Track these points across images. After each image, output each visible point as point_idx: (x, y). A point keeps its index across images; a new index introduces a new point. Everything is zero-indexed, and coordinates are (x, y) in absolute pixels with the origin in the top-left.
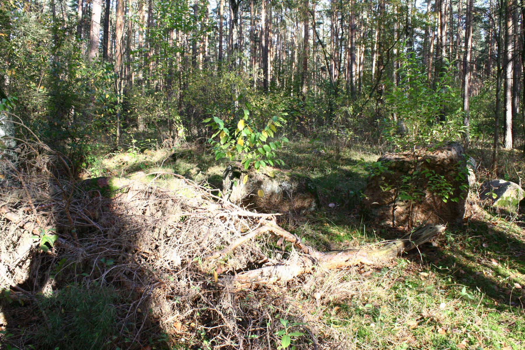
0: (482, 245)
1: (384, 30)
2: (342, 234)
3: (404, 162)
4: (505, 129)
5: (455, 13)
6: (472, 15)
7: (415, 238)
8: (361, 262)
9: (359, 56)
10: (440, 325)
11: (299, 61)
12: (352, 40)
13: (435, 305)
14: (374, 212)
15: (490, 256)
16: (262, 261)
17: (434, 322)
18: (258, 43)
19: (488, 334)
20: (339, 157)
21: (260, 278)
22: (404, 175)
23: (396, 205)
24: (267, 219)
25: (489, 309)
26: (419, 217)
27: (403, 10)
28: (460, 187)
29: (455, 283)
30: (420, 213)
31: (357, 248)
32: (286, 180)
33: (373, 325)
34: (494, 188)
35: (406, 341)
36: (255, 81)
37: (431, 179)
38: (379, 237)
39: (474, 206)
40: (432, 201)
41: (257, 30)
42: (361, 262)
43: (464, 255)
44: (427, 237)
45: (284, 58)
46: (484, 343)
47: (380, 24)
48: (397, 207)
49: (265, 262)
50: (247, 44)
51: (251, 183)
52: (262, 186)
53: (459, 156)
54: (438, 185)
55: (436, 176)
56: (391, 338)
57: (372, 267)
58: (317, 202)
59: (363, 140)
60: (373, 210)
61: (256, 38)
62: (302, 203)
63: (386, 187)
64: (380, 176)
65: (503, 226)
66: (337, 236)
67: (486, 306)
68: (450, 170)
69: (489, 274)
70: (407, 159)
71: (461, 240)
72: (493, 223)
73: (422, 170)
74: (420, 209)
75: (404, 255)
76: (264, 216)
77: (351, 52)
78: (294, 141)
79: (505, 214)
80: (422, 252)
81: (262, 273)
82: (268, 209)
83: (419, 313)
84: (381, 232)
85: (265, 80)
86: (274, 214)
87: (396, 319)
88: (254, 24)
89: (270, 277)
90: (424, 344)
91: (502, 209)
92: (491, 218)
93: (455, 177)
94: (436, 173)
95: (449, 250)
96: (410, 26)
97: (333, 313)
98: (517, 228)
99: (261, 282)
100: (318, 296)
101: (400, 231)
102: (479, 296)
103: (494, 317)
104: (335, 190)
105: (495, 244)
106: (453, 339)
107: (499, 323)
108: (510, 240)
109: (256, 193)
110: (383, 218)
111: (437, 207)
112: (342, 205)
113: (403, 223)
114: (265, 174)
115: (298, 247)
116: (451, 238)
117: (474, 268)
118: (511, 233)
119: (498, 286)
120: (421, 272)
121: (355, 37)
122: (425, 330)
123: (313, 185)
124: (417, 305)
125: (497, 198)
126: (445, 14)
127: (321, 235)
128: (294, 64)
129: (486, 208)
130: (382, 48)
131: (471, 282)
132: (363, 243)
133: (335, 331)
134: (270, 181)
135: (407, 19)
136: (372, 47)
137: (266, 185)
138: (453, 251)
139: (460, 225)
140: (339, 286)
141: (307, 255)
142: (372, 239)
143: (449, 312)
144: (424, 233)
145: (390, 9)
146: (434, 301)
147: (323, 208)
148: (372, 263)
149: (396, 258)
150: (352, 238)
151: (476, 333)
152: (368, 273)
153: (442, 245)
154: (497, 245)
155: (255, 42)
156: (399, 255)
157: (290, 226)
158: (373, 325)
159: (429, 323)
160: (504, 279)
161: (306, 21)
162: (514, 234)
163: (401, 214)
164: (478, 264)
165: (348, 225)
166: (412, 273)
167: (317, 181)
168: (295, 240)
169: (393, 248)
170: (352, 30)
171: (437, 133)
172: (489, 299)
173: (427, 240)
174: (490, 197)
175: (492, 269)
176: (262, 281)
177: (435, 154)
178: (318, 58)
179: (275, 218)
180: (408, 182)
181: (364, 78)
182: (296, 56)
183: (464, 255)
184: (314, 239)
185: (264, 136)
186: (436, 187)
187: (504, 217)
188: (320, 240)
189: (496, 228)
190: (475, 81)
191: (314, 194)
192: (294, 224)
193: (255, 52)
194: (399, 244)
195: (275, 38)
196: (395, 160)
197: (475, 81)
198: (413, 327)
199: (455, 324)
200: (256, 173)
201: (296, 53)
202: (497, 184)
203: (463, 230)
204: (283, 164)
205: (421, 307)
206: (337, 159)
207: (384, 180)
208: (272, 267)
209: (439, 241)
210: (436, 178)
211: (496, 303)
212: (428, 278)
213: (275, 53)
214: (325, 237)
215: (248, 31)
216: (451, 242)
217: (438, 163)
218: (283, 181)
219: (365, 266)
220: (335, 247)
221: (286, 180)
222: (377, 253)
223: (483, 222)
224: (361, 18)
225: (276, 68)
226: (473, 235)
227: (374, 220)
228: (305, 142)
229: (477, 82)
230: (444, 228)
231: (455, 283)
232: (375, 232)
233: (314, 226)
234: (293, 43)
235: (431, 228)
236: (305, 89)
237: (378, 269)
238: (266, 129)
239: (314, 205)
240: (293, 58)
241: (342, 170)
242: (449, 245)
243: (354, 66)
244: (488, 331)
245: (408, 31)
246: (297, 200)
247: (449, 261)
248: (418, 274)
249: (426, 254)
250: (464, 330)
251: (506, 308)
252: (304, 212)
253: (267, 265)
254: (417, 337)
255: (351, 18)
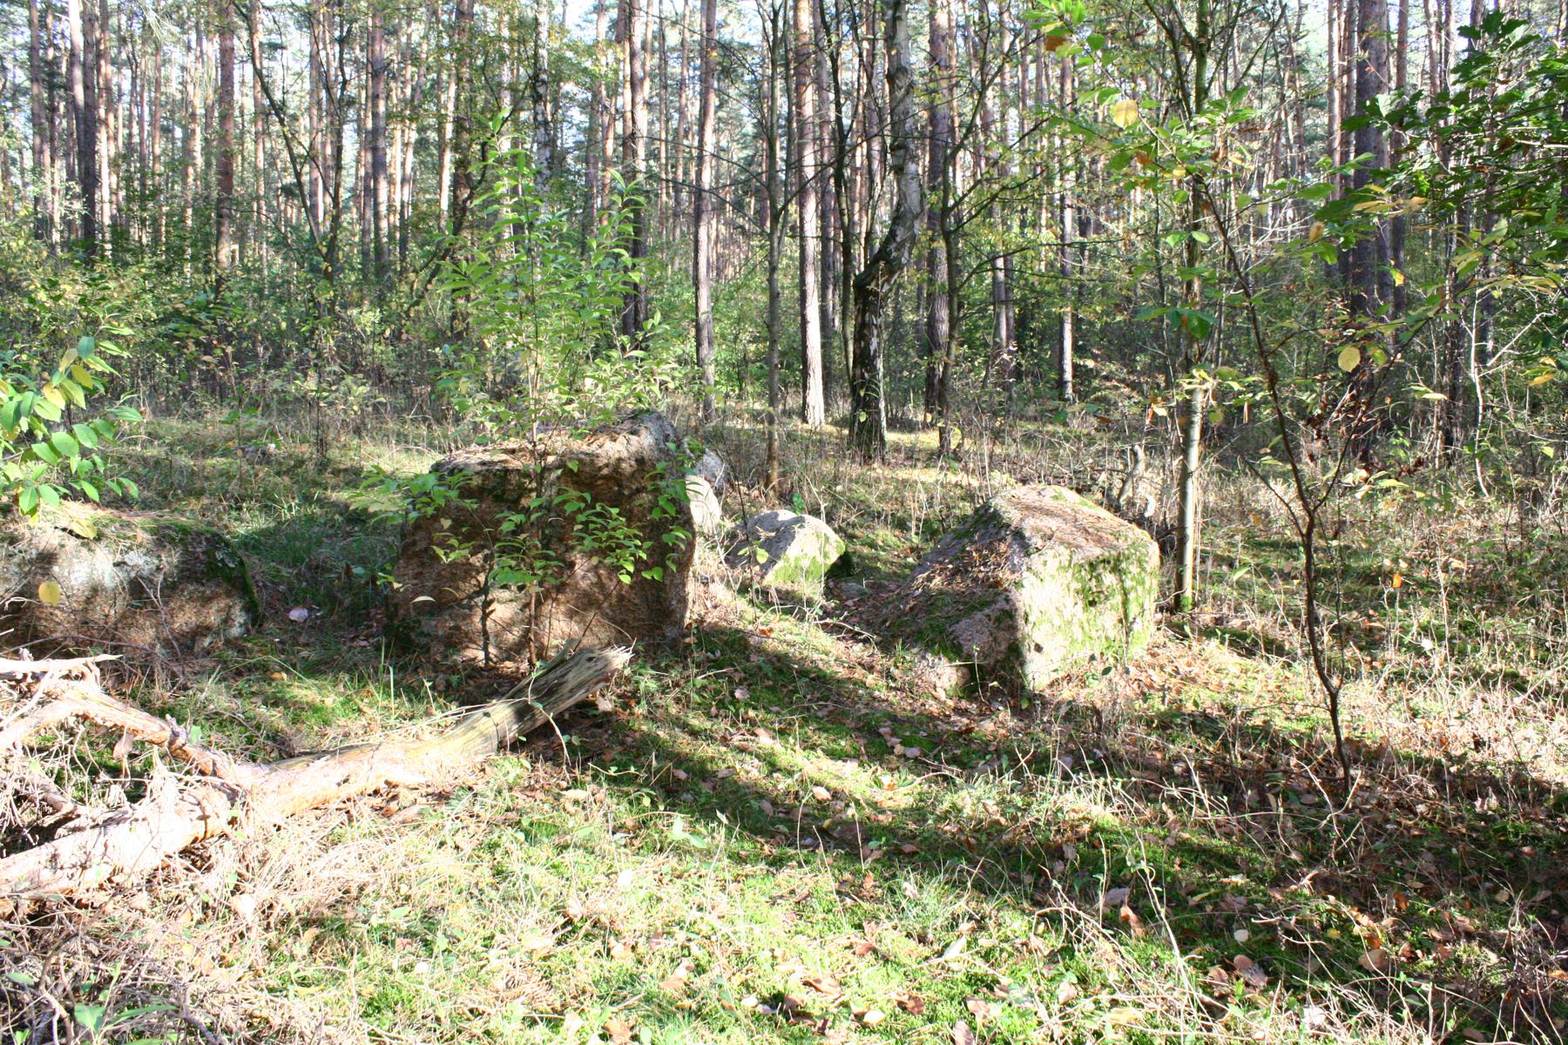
0: (732, 694)
1: (470, 81)
2: (329, 702)
3: (506, 471)
4: (805, 374)
5: (674, 49)
6: (719, 60)
7: (547, 692)
8: (387, 783)
9: (399, 157)
10: (618, 935)
11: (208, 164)
12: (375, 106)
13: (604, 880)
14: (428, 624)
15: (753, 723)
16: (58, 816)
17: (600, 930)
18: (62, 92)
19: (743, 935)
20: (323, 465)
21: (46, 875)
22: (509, 509)
23: (492, 601)
24: (67, 677)
25: (748, 868)
26: (559, 628)
27: (526, 28)
28: (665, 538)
29: (662, 808)
30: (561, 617)
31: (375, 738)
32: (140, 546)
33: (422, 967)
34: (763, 534)
35: (523, 998)
36: (57, 219)
37: (581, 518)
38: (441, 700)
39: (712, 586)
40: (595, 580)
41: (57, 48)
42: (387, 783)
43: (685, 727)
44: (580, 686)
45: (158, 151)
46: (734, 962)
47: (459, 62)
48: (494, 606)
49: (67, 818)
50: (18, 90)
51: (16, 560)
52: (56, 569)
53: (660, 450)
54: (603, 536)
55: (598, 509)
56: (479, 999)
57: (424, 791)
58: (250, 608)
59: (404, 410)
60: (424, 620)
61: (52, 75)
62: (198, 613)
63: (452, 548)
64: (435, 518)
65: (788, 637)
66: (315, 709)
67: (738, 859)
68: (638, 491)
69: (750, 771)
70: (515, 464)
71: (676, 685)
72: (763, 632)
73: (559, 492)
74: (562, 608)
75: (516, 747)
76: (55, 667)
77: (373, 141)
78: (184, 418)
79: (791, 603)
80: (572, 733)
81: (54, 857)
82: (84, 643)
83: (559, 909)
84: (449, 685)
85: (89, 221)
86: (89, 660)
87: (492, 937)
88: (44, 26)
89: (84, 867)
90: (574, 998)
91: (787, 592)
92: (756, 618)
93: (650, 510)
94: (595, 500)
95: (646, 718)
96: (544, 77)
97: (301, 949)
98: (825, 641)
99: (54, 887)
100: (246, 905)
101: (506, 677)
102: (718, 835)
103: (761, 883)
104: (309, 568)
105: (768, 688)
106: (651, 969)
107: (773, 902)
108: (803, 673)
109: (34, 595)
110: (455, 641)
111: (608, 596)
112: (331, 612)
113: (513, 652)
114: (64, 530)
115: (175, 756)
116: (648, 683)
117: (712, 759)
118: (805, 653)
119: (774, 803)
120: (568, 789)
121: (388, 97)
122: (577, 956)
123: (232, 555)
124: (552, 884)
125: (771, 562)
126: (644, 48)
127: (263, 709)
128: (191, 170)
129: (743, 590)
130: (466, 136)
131: (703, 800)
132: (392, 721)
133: (300, 1009)
134: (84, 551)
135: (536, 54)
136: (440, 130)
137: (71, 565)
138: (654, 720)
139: (674, 644)
140: (320, 863)
141: (209, 779)
142: (422, 708)
143: (642, 894)
144: (570, 675)
145: (490, 20)
146: (604, 869)
147: (270, 626)
148: (423, 780)
149: (493, 756)
150: (360, 710)
151: (713, 938)
152: (411, 813)
153: (626, 706)
154: (772, 689)
155: (51, 87)
156: (501, 746)
157: (161, 692)
158: (422, 967)
159: (586, 936)
160: (789, 781)
161: (226, 32)
162: (816, 656)
163: (507, 627)
164: (723, 749)
165: (349, 671)
166: (539, 795)
167: (252, 544)
168: (167, 734)
169: (482, 728)
170: (375, 75)
171: (605, 385)
172: (751, 839)
173: (580, 696)
174: (752, 559)
175: (758, 756)
176: (55, 886)
177: (594, 446)
178: (272, 159)
179: (97, 671)
180: (519, 529)
181: (414, 225)
182: (197, 144)
183: (685, 727)
184: (240, 724)
185: (51, 404)
186: (598, 540)
187: (789, 612)
188: (258, 727)
189: (771, 645)
190: (729, 242)
191: (238, 584)
192: (173, 685)
193: (52, 122)
194: (500, 715)
195: (123, 81)
196: (479, 468)
197: (729, 242)
198: (544, 953)
199: (659, 924)
200: (30, 528)
201: (199, 136)
202: (769, 522)
203: (680, 654)
204: (134, 490)
205: (565, 891)
206: (320, 472)
207: (451, 529)
208: (89, 836)
209: (619, 697)
210: (599, 515)
211: (766, 847)
212: (591, 807)
213: (123, 132)
214: (275, 718)
215: (23, 47)
216: (650, 696)
217: (605, 471)
218: (130, 548)
219: (402, 792)
220: (301, 743)
221: (140, 546)
222: (447, 748)
223: (738, 631)
224: (404, 39)
225: (129, 180)
226: (709, 669)
227: (428, 651)
228: (215, 421)
229: (735, 242)
230: (628, 656)
231: (662, 808)
232: (428, 684)
233: (240, 684)
234: (186, 103)
235: (590, 659)
236: (226, 250)
237: (442, 797)
238: (56, 381)
239: (239, 617)
240: (187, 151)
241: (334, 504)
242: (643, 702)
243: (383, 186)
244: (742, 926)
245: (541, 90)
246: (181, 608)
247: (640, 748)
248: (557, 798)
249: (581, 735)
250: (681, 936)
251: (790, 858)
252: (207, 642)
253: (75, 830)
254: (554, 979)
255: (373, 39)
